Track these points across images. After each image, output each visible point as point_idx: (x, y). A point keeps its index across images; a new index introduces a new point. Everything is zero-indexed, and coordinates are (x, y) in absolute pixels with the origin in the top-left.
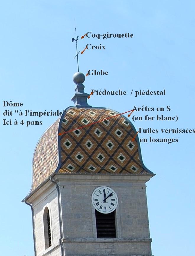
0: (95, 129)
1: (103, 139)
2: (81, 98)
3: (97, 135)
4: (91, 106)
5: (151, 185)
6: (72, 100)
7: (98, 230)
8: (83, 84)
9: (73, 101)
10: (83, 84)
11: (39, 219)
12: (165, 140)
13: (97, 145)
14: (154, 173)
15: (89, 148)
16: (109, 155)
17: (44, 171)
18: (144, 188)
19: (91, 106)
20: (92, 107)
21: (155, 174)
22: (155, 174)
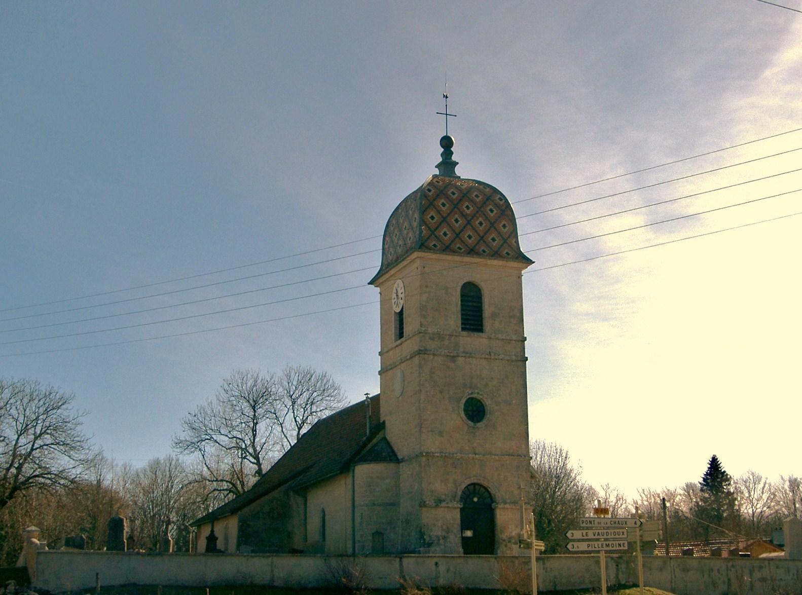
0: (456, 198)
1: (474, 216)
2: (447, 164)
3: (506, 223)
4: (460, 177)
5: (527, 274)
6: (436, 167)
7: (480, 305)
8: (452, 149)
9: (437, 169)
10: (452, 149)
11: (208, 405)
12: (299, 473)
13: (496, 225)
14: (533, 261)
15: (445, 230)
16: (460, 239)
17: (392, 252)
18: (520, 277)
19: (460, 177)
20: (461, 178)
21: (534, 262)
22: (534, 262)
